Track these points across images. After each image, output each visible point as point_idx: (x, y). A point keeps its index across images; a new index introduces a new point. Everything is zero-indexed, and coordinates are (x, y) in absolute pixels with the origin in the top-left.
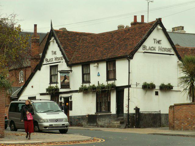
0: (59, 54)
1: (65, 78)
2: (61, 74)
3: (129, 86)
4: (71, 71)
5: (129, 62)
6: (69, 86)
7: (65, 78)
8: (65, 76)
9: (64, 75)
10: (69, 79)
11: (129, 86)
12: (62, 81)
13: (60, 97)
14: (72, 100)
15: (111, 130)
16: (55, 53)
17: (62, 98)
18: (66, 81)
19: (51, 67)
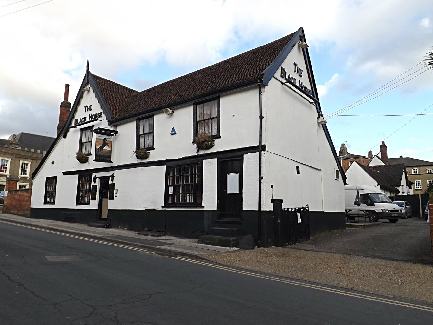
0: (97, 109)
1: (105, 143)
2: (98, 135)
3: (261, 148)
4: (116, 132)
5: (260, 93)
6: (110, 157)
7: (105, 143)
8: (105, 139)
9: (103, 137)
10: (110, 147)
11: (261, 148)
12: (98, 147)
13: (93, 176)
14: (113, 183)
15: (98, 196)
16: (90, 108)
17: (98, 180)
18: (106, 148)
19: (82, 130)
